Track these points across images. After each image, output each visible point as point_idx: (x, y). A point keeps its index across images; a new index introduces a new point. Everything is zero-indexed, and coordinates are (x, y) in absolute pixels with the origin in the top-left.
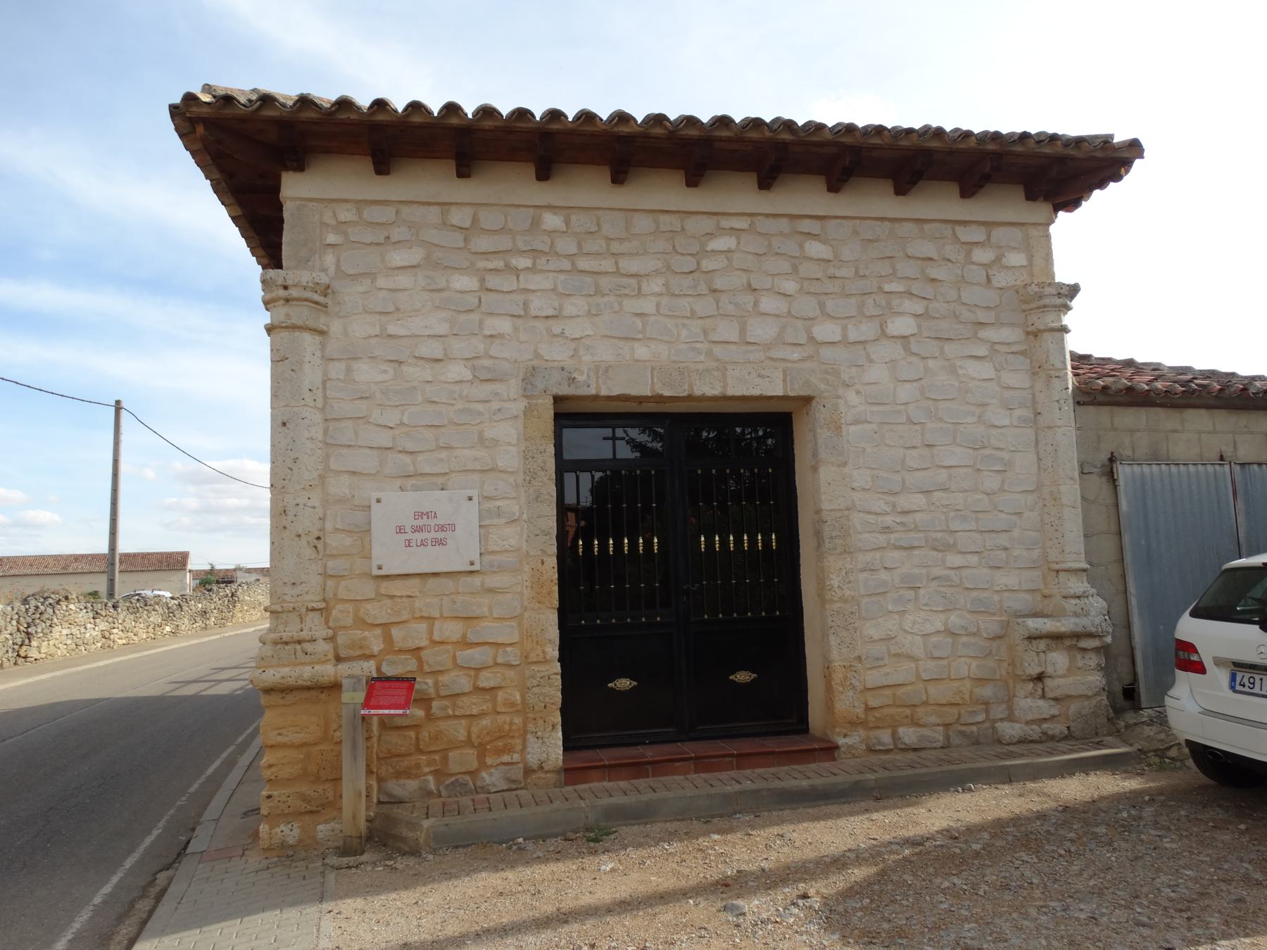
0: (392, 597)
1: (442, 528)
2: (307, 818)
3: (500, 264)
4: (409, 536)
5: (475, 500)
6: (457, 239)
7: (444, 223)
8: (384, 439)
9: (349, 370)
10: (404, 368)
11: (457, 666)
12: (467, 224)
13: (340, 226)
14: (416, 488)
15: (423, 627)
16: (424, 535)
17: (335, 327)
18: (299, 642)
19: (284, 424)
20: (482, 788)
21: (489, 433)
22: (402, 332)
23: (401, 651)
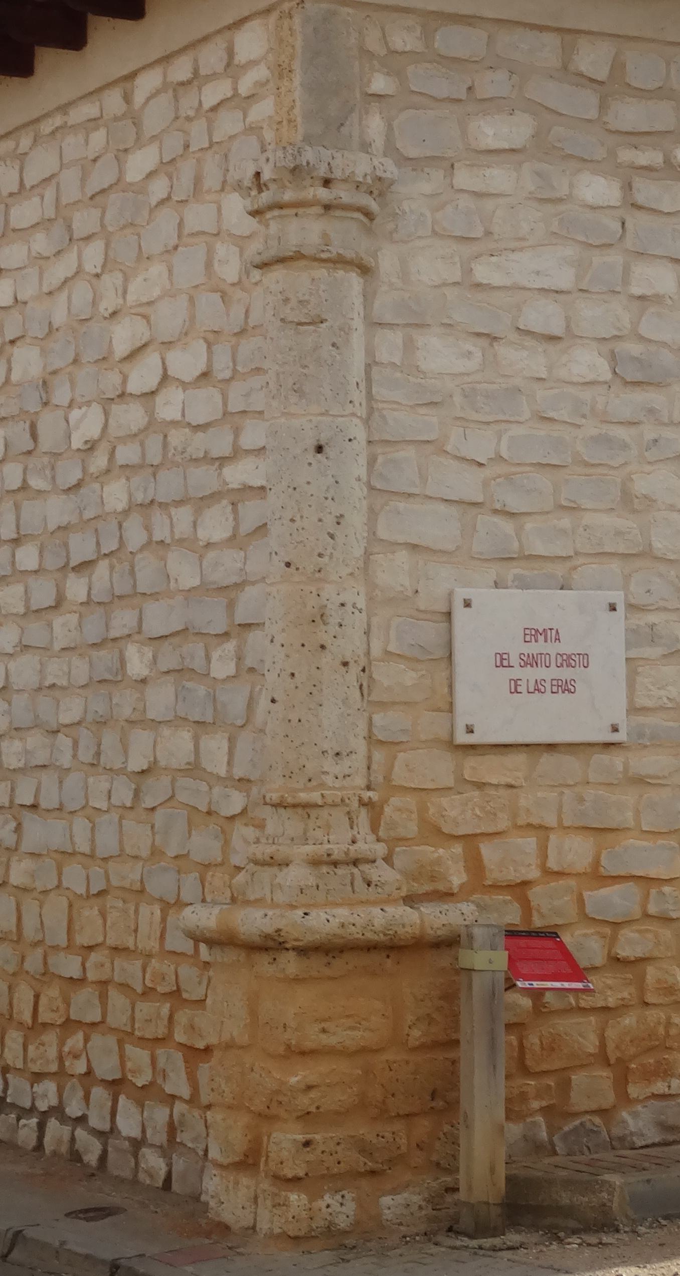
0: (480, 786)
1: (567, 661)
2: (364, 1183)
3: (654, 157)
4: (517, 672)
5: (621, 608)
6: (586, 102)
7: (565, 68)
8: (468, 484)
9: (409, 346)
10: (503, 351)
11: (587, 919)
12: (602, 74)
13: (393, 61)
14: (523, 584)
15: (530, 843)
16: (540, 673)
17: (387, 262)
18: (355, 863)
19: (319, 449)
20: (622, 1139)
21: (641, 486)
22: (497, 279)
23: (496, 887)
